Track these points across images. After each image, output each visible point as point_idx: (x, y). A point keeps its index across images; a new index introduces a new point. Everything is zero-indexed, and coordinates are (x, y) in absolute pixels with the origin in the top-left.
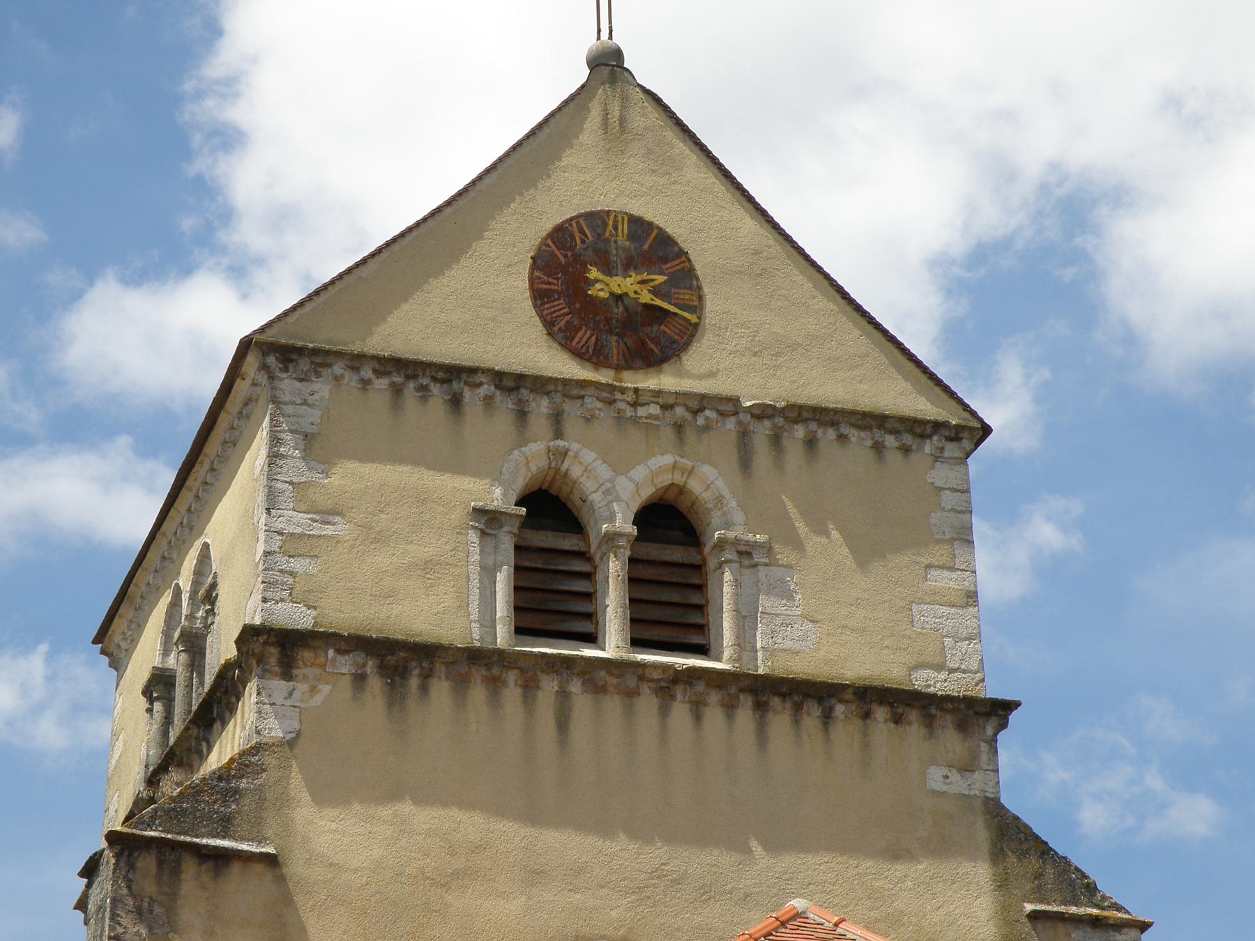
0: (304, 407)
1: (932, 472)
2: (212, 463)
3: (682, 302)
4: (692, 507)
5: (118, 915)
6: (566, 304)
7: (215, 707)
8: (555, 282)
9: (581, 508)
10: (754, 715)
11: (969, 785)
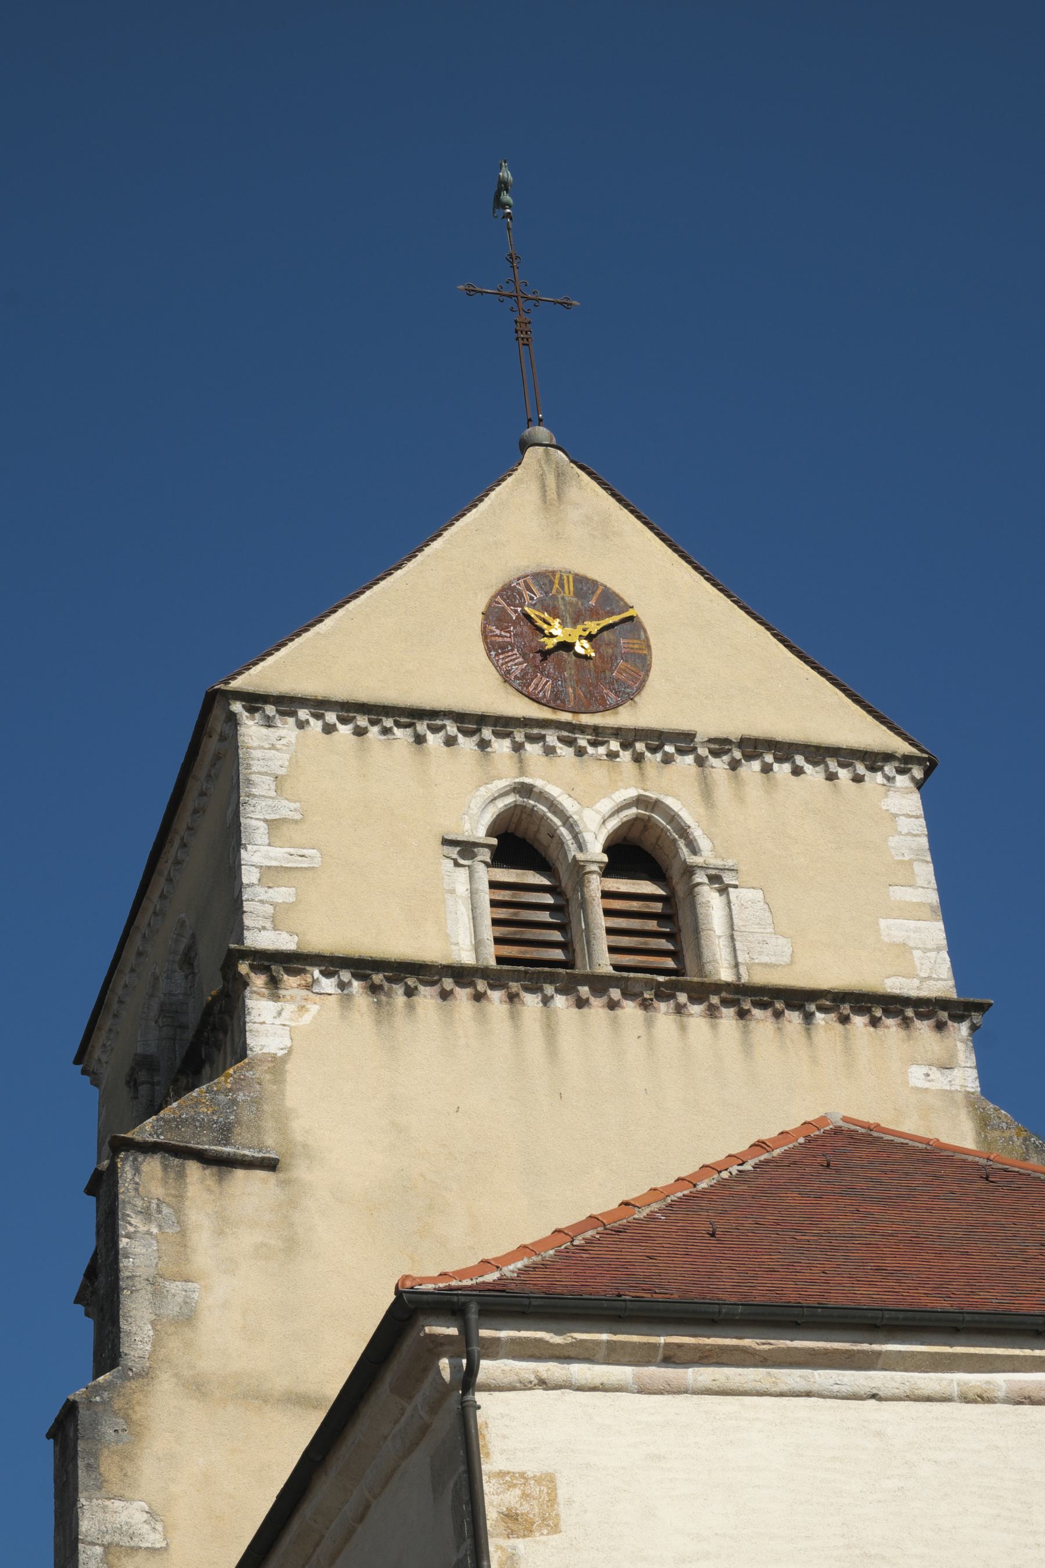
0: (273, 751)
1: (886, 800)
2: (182, 838)
3: (632, 651)
4: (657, 843)
5: (128, 1215)
6: (520, 654)
7: (203, 1049)
8: (508, 635)
9: (549, 846)
10: (737, 1024)
11: (950, 1081)
